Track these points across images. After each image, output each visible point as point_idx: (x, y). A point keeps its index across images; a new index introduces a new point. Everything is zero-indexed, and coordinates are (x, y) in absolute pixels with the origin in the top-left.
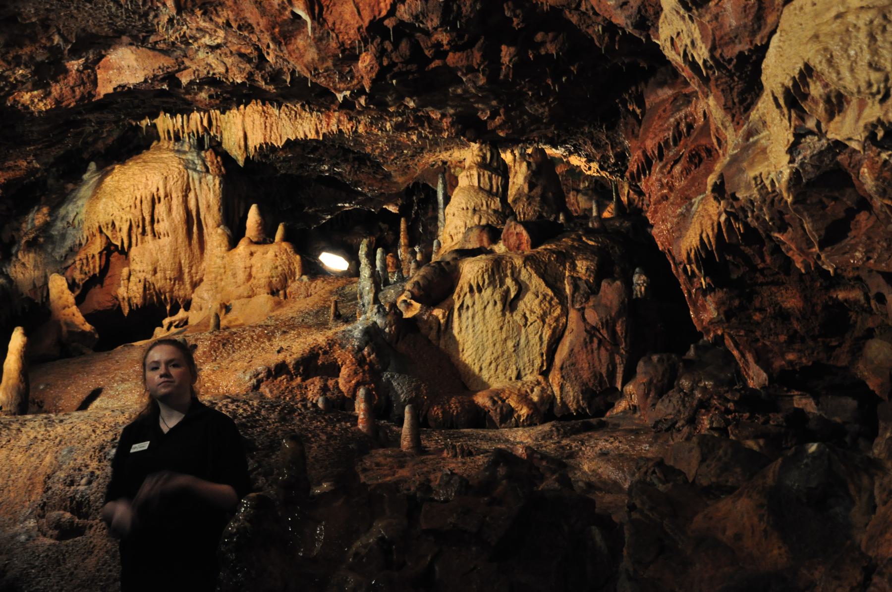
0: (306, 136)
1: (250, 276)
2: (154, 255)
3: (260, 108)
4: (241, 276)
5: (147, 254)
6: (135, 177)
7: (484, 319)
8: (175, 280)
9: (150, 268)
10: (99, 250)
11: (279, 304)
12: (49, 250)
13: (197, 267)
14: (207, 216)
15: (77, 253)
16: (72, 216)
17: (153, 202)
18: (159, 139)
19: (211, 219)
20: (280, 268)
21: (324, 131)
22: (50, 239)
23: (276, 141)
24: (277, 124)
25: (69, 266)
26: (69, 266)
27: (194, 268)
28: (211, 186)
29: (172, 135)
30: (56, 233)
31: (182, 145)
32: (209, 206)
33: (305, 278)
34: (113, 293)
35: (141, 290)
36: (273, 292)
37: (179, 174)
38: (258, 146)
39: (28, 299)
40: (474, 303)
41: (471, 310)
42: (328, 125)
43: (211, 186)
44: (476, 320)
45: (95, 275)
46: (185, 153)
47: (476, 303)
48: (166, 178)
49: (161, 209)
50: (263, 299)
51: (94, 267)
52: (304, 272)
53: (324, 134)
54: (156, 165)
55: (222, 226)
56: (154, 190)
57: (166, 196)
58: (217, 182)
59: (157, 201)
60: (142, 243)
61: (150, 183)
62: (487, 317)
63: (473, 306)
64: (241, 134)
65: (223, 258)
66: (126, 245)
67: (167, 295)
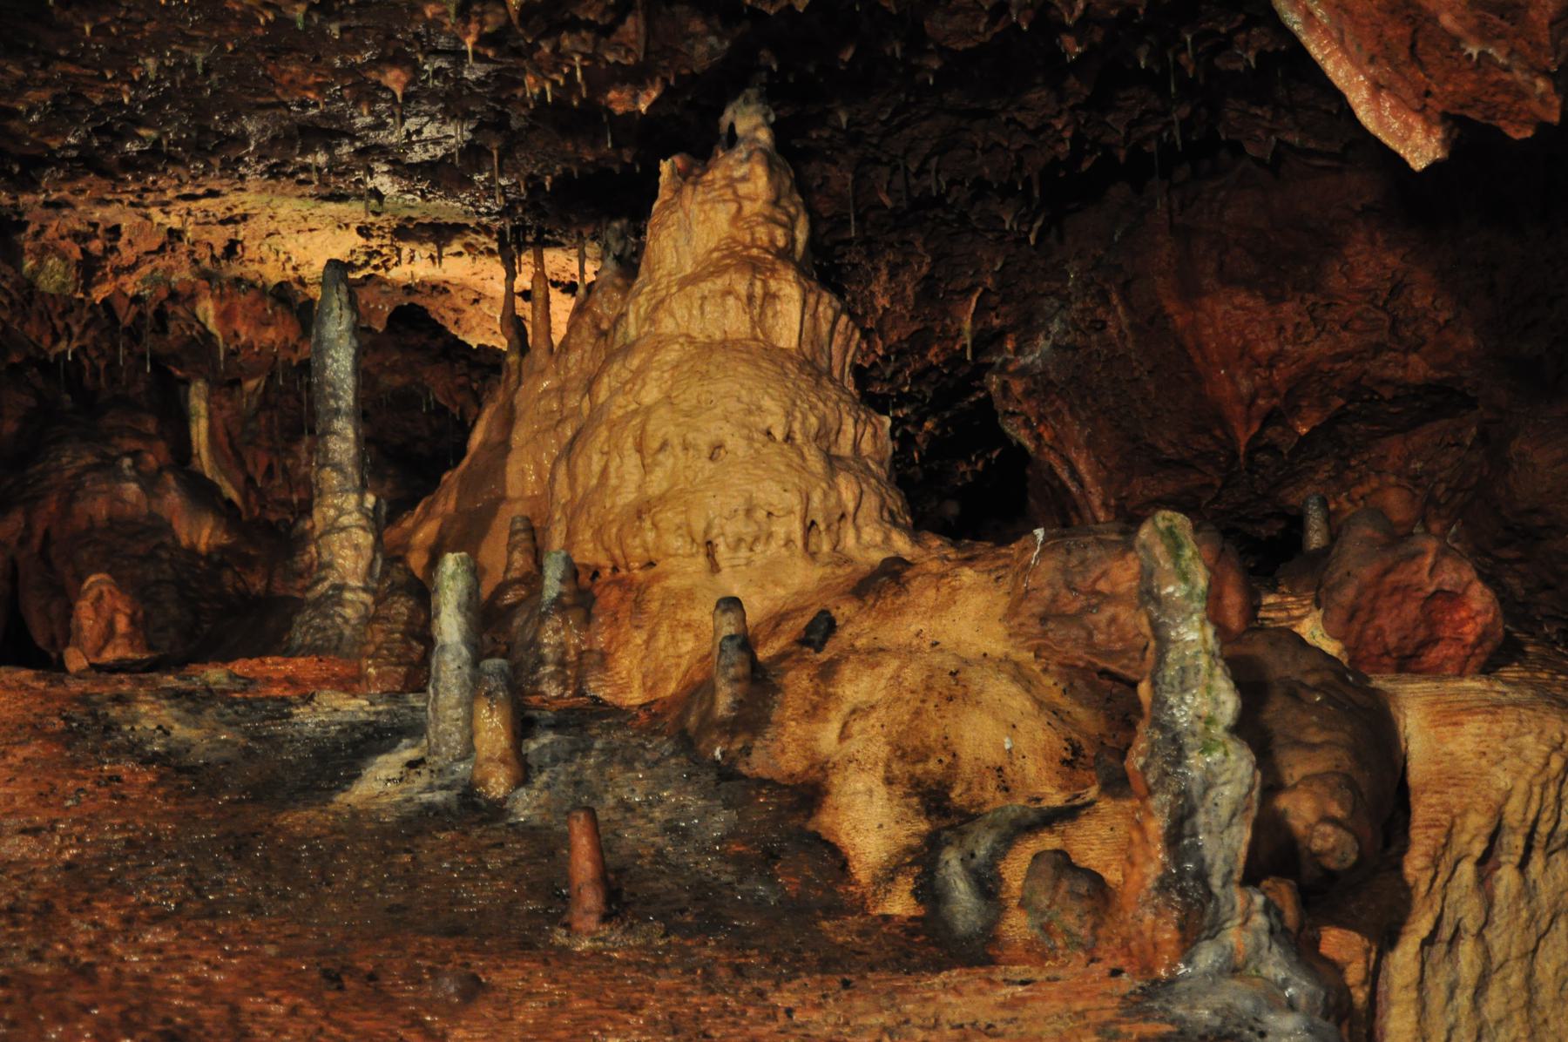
7: (1530, 1005)
40: (1487, 922)
41: (1467, 950)
44: (1494, 1006)
47: (1499, 920)
62: (1546, 995)
63: (1480, 936)
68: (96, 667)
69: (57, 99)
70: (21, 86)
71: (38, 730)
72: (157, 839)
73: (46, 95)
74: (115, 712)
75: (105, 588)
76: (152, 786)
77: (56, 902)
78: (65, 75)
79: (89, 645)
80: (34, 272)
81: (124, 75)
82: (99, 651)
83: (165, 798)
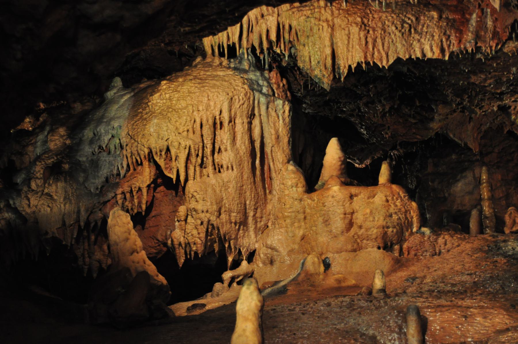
0: (424, 55)
1: (351, 224)
2: (218, 192)
3: (359, 19)
4: (338, 224)
5: (210, 190)
6: (193, 96)
8: (241, 224)
9: (215, 207)
10: (148, 183)
11: (399, 264)
12: (81, 180)
13: (262, 211)
14: (275, 149)
15: (117, 185)
16: (106, 139)
17: (216, 125)
18: (204, 55)
19: (279, 155)
20: (395, 217)
21: (455, 48)
22: (77, 166)
23: (381, 60)
24: (383, 40)
25: (109, 201)
26: (109, 201)
27: (259, 210)
28: (280, 113)
29: (216, 51)
30: (84, 159)
31: (240, 62)
32: (278, 137)
33: (426, 230)
34: (160, 238)
35: (203, 235)
36: (387, 246)
37: (246, 95)
38: (353, 67)
39: (54, 238)
42: (460, 42)
43: (280, 113)
45: (139, 213)
46: (246, 72)
48: (232, 99)
49: (224, 136)
50: (373, 256)
51: (140, 203)
52: (423, 222)
53: (452, 54)
54: (218, 83)
55: (291, 162)
56: (218, 113)
57: (230, 121)
58: (287, 108)
59: (218, 126)
60: (201, 176)
61: (212, 103)
64: (328, 51)
65: (301, 200)
66: (182, 178)
67: (232, 242)
68: (512, 232)
69: (496, 81)
70: (485, 80)
71: (481, 250)
72: (498, 276)
73: (492, 81)
74: (502, 245)
75: (512, 211)
76: (505, 263)
77: (468, 290)
78: (495, 75)
79: (509, 226)
80: (515, 119)
81: (509, 72)
82: (512, 228)
83: (507, 266)
